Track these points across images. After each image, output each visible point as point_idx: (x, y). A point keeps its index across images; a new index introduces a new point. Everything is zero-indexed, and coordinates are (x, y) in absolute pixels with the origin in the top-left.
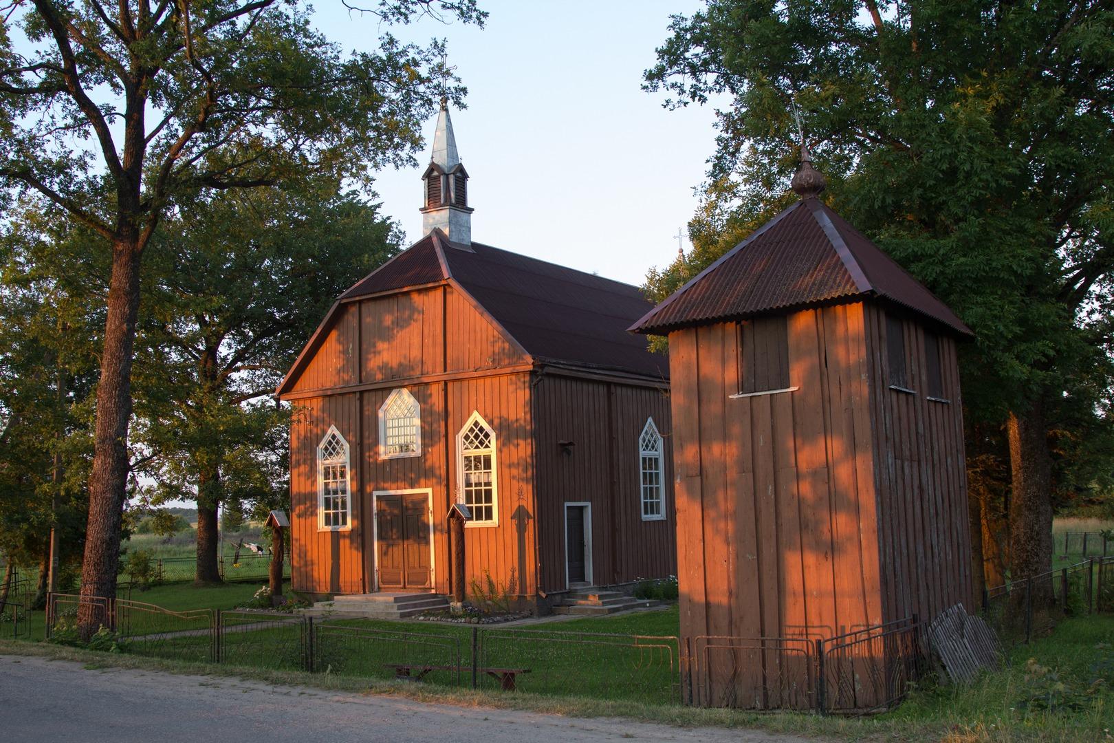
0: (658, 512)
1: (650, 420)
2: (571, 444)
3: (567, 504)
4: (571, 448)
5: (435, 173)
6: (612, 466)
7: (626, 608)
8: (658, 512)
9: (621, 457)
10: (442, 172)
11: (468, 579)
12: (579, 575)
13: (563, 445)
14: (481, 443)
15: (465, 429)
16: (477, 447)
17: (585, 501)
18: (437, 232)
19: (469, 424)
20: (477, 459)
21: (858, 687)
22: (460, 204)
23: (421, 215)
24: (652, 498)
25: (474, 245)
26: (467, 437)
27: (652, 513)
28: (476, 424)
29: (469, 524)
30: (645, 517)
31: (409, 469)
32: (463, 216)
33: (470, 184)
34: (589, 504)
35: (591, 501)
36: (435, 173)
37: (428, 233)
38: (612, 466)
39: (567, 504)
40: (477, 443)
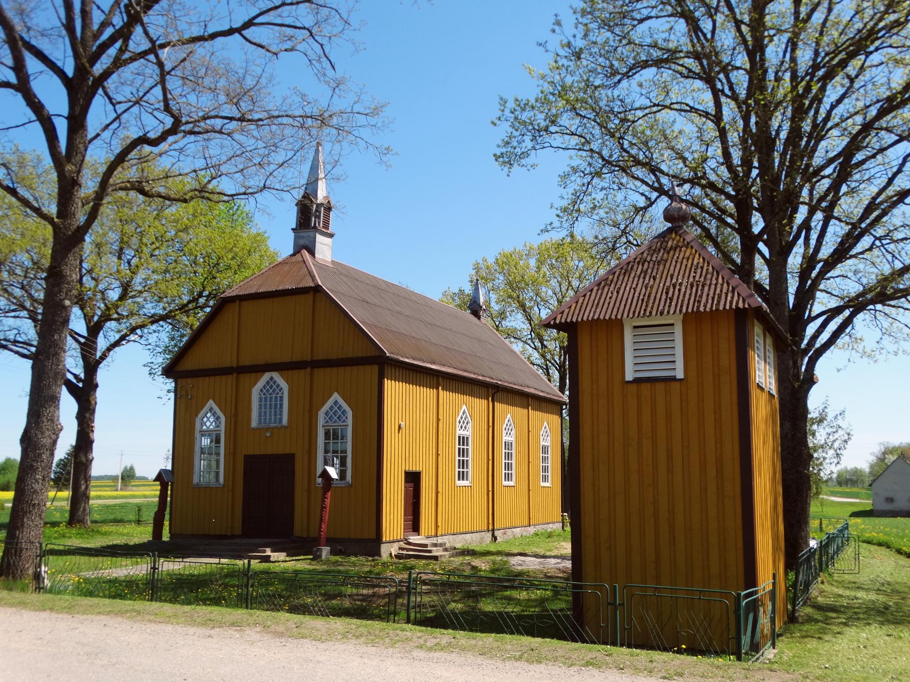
27: (463, 479)
28: (336, 403)
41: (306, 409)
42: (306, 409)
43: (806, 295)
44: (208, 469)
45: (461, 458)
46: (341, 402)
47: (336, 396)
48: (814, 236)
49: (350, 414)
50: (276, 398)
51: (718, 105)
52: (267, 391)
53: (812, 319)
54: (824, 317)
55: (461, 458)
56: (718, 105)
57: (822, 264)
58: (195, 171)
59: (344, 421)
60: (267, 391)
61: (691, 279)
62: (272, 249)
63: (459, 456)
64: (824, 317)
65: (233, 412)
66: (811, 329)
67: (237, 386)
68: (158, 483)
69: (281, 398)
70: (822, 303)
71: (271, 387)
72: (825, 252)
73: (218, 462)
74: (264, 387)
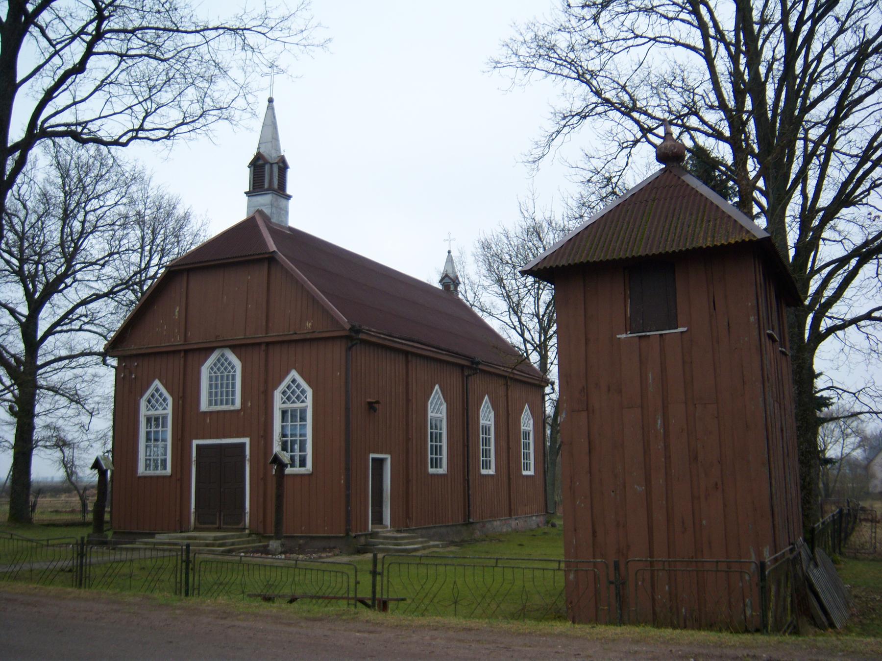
0: (441, 467)
1: (437, 387)
2: (377, 402)
3: (372, 456)
4: (376, 405)
5: (261, 162)
6: (407, 424)
7: (424, 548)
8: (441, 467)
9: (414, 416)
10: (266, 162)
11: (167, 541)
12: (378, 519)
13: (370, 403)
14: (298, 398)
15: (283, 386)
16: (294, 402)
17: (386, 453)
18: (260, 212)
19: (287, 381)
20: (294, 411)
21: (748, 612)
22: (281, 190)
23: (245, 198)
24: (436, 454)
25: (291, 229)
26: (284, 393)
27: (436, 467)
28: (294, 381)
29: (289, 470)
30: (432, 471)
31: (222, 422)
32: (283, 201)
33: (290, 175)
34: (388, 457)
35: (390, 453)
36: (261, 162)
37: (251, 215)
38: (407, 424)
39: (372, 456)
40: (294, 398)
41: (259, 392)
42: (259, 392)
43: (809, 244)
44: (155, 457)
45: (434, 443)
46: (300, 380)
47: (294, 374)
48: (812, 183)
49: (309, 392)
50: (228, 376)
51: (706, 44)
52: (219, 369)
53: (814, 272)
54: (833, 266)
55: (438, 444)
56: (706, 44)
57: (821, 214)
58: (130, 107)
59: (165, 409)
60: (219, 369)
61: (653, 195)
62: (127, 168)
63: (431, 441)
64: (833, 266)
65: (181, 395)
66: (814, 285)
67: (266, 365)
68: (96, 471)
69: (234, 377)
70: (828, 251)
71: (222, 365)
72: (826, 199)
73: (165, 448)
74: (215, 365)
